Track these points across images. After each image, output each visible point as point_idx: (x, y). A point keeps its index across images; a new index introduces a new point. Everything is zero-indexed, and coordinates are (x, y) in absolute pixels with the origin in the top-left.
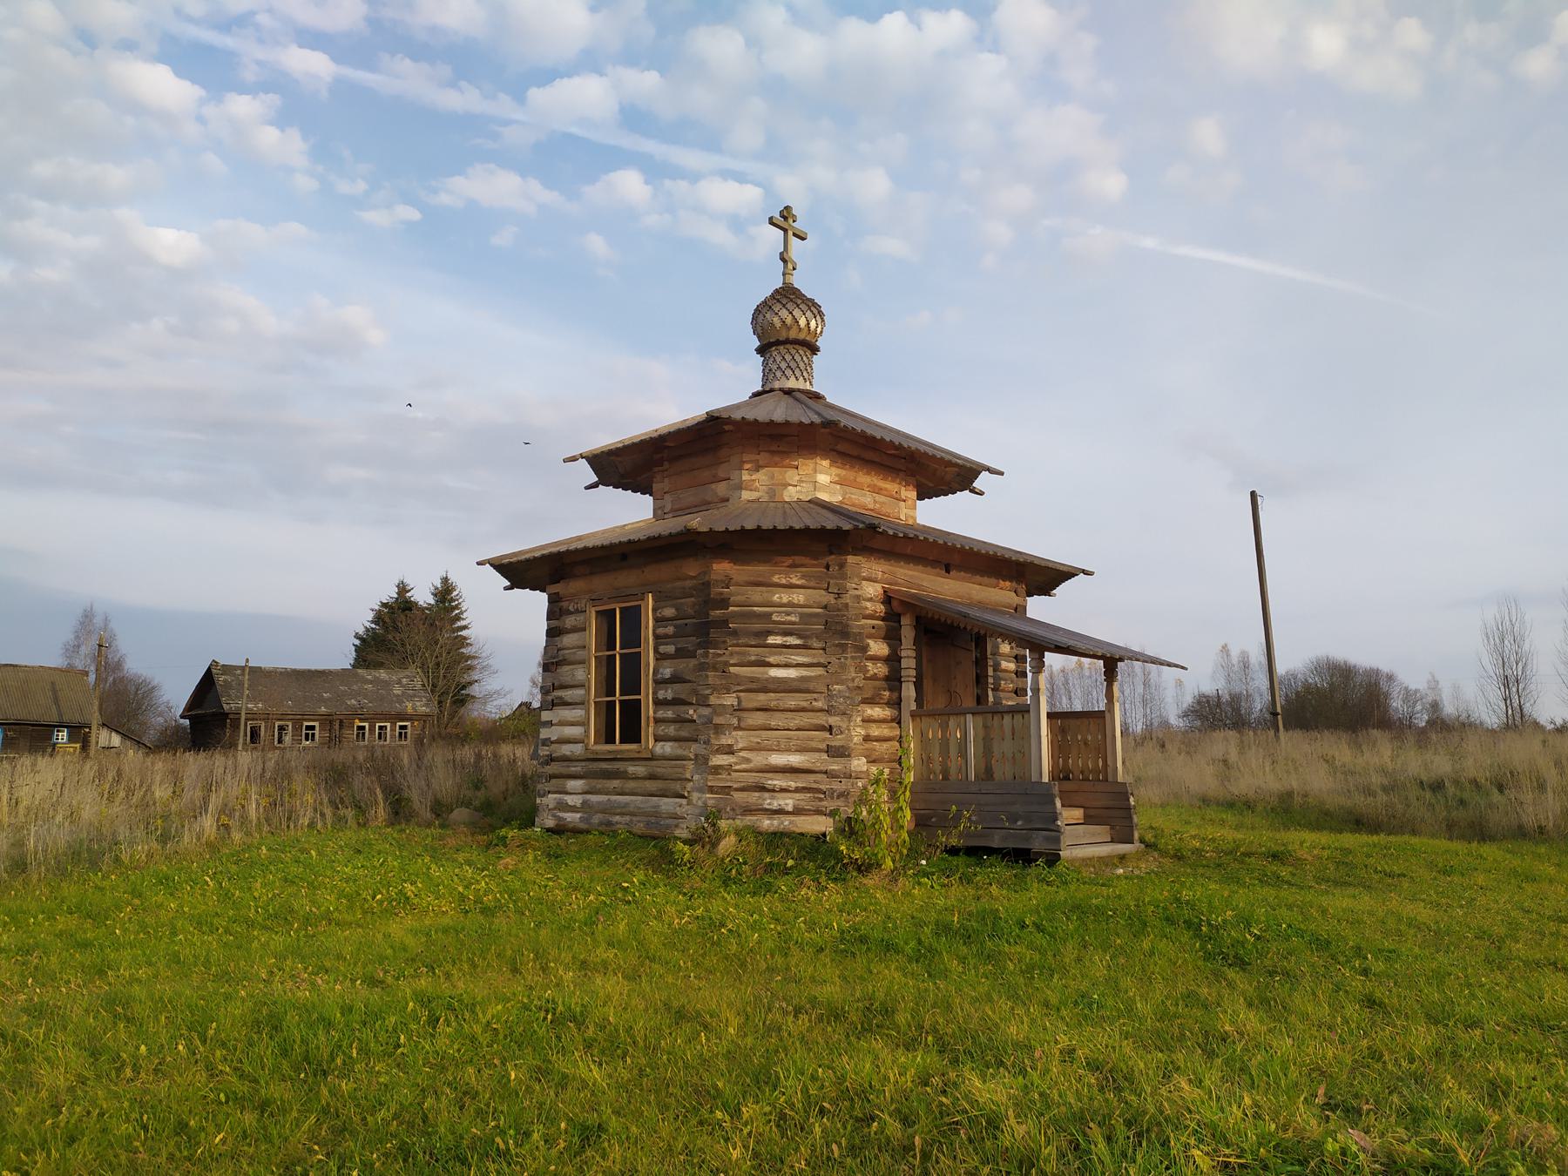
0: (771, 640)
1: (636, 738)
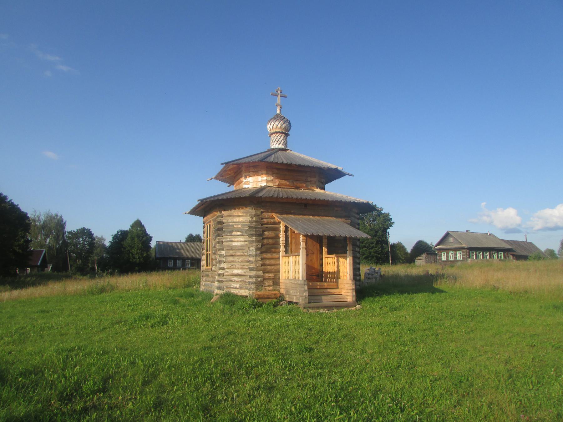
0: (233, 233)
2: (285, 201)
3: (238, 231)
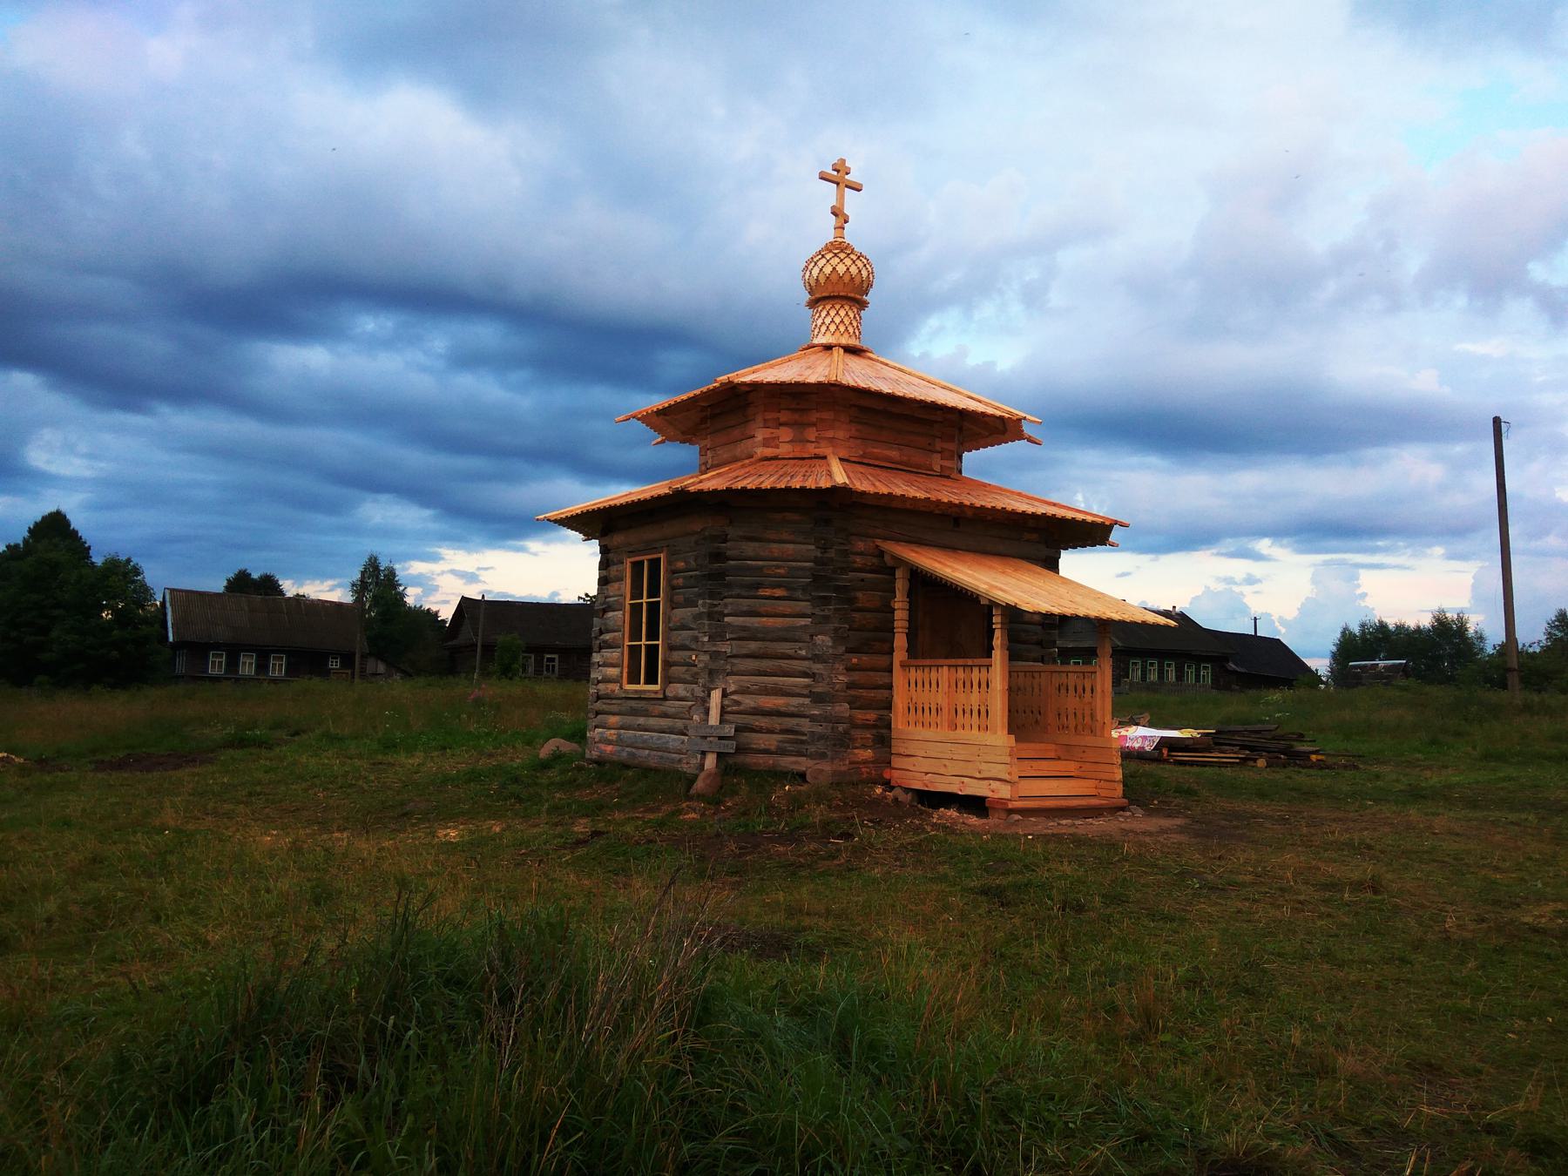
0: (761, 592)
1: (652, 679)
2: (908, 506)
3: (779, 586)
